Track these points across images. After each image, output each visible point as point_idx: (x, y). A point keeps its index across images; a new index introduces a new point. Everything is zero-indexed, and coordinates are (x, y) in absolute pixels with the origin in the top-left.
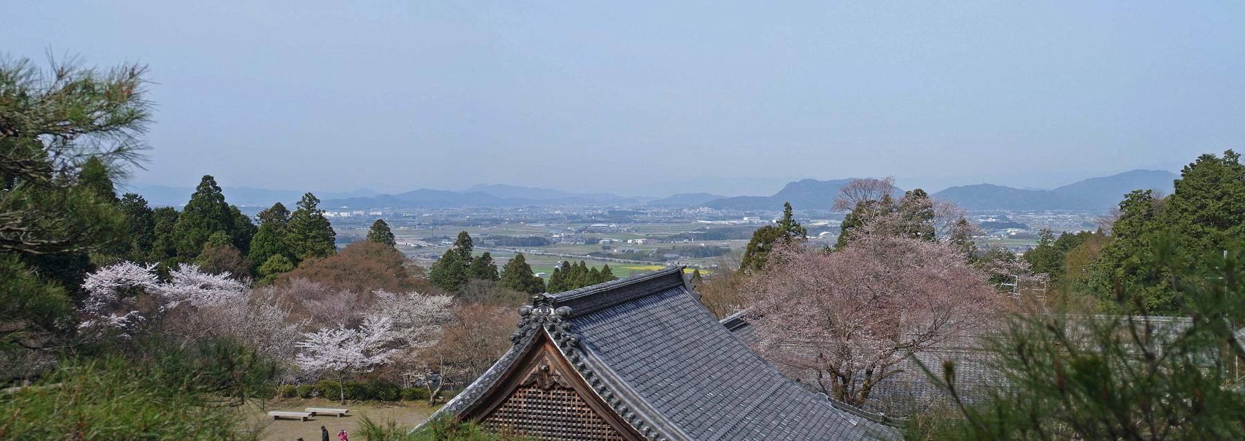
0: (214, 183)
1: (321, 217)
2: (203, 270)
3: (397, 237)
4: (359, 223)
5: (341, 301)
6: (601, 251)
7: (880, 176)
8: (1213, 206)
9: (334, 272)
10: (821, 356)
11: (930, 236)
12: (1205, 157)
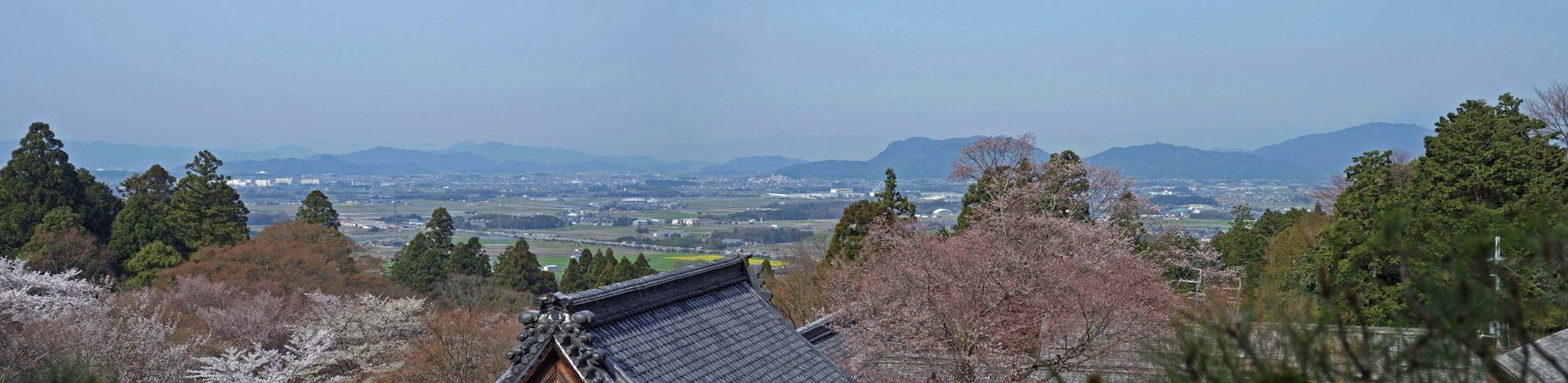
0: (49, 134)
1: (225, 187)
2: (32, 267)
3: (342, 215)
4: (284, 196)
5: (257, 309)
6: (635, 235)
7: (1016, 135)
8: (1480, 173)
9: (246, 267)
10: (934, 376)
11: (1083, 214)
12: (1471, 105)
